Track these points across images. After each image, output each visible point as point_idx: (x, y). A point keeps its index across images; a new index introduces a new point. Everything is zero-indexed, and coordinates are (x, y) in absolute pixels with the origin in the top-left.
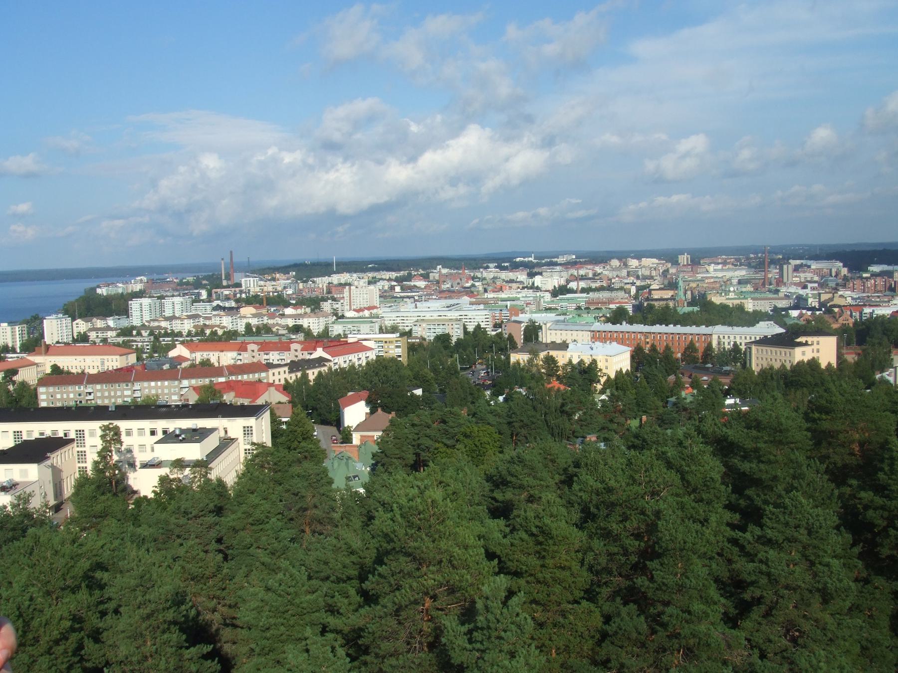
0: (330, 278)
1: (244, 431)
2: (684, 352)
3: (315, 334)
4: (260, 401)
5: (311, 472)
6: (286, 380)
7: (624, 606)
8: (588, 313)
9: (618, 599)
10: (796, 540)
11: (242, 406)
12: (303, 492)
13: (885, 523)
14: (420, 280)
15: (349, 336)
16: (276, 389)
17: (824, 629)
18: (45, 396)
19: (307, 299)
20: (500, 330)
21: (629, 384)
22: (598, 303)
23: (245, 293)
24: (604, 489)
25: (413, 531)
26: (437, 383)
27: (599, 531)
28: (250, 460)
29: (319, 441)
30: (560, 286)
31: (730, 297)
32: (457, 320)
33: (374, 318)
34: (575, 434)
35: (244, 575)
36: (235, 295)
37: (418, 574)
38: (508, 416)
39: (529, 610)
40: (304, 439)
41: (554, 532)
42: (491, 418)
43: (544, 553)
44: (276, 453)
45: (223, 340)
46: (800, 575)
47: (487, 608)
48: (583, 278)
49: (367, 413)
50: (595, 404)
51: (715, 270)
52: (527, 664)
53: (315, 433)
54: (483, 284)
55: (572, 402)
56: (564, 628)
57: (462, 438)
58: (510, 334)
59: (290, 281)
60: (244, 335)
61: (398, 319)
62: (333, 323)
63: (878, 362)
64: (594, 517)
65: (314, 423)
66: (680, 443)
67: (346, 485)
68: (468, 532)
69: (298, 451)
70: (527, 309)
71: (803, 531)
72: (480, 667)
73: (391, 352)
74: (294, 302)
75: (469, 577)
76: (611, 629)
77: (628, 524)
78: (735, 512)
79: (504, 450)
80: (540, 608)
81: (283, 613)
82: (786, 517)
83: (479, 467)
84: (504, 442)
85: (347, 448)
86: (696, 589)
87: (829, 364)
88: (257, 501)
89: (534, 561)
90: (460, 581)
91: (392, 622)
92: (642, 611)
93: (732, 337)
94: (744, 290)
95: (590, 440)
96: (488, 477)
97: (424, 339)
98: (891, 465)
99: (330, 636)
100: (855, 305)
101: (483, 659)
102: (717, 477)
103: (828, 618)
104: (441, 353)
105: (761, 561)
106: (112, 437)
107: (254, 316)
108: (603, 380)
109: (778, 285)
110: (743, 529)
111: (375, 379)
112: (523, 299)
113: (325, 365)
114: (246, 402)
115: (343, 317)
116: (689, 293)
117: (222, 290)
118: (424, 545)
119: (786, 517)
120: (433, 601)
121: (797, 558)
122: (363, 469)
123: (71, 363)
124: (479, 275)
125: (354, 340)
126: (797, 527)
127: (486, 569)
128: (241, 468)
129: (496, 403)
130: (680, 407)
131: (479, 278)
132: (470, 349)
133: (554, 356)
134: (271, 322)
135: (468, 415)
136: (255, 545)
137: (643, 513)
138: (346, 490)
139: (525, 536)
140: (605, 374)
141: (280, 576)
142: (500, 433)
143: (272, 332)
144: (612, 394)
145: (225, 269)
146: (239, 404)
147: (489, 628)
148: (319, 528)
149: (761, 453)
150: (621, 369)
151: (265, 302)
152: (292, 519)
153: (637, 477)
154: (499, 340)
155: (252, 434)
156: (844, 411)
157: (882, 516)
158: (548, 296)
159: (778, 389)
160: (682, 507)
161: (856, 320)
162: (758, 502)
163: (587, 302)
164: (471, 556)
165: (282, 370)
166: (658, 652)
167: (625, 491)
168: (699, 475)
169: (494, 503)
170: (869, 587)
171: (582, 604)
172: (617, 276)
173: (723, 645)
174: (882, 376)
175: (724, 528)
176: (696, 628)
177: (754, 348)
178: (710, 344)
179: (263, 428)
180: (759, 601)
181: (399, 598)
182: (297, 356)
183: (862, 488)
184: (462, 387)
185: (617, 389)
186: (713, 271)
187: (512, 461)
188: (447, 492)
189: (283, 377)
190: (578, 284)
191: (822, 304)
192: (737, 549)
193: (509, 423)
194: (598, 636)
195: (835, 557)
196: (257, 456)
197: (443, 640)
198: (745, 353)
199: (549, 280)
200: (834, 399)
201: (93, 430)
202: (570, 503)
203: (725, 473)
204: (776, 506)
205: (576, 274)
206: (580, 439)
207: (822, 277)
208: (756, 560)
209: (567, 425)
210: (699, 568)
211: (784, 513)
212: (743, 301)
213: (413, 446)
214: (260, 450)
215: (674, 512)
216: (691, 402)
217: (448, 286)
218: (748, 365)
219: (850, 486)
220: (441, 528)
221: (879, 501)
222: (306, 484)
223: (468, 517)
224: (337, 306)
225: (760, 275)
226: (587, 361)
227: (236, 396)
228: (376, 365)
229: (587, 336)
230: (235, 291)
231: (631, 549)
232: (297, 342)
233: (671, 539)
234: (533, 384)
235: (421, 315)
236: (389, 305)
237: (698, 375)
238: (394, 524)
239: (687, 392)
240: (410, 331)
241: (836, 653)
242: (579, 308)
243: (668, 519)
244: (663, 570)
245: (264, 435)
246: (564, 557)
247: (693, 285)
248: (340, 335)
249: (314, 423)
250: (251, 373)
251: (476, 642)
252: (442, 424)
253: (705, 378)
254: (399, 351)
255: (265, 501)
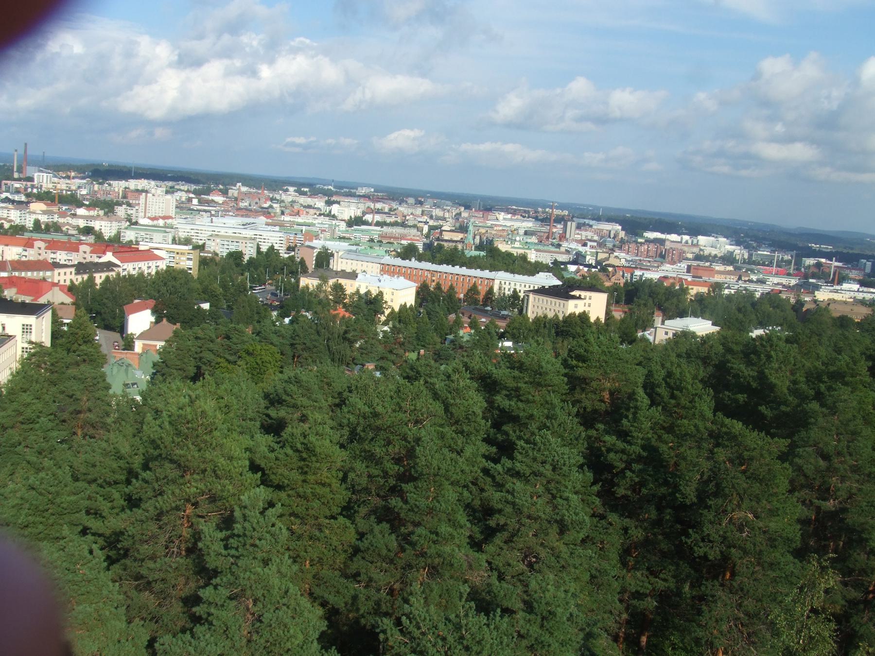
0: (127, 183)
1: (23, 329)
2: (467, 293)
3: (106, 238)
4: (42, 300)
5: (88, 375)
6: (71, 281)
7: (378, 525)
8: (380, 246)
9: (373, 518)
10: (541, 475)
11: (23, 304)
12: (78, 394)
13: (623, 466)
14: (219, 195)
15: (141, 243)
16: (61, 290)
17: (558, 557)
19: (101, 202)
20: (293, 253)
21: (411, 318)
22: (391, 238)
23: (37, 188)
24: (371, 413)
25: (180, 439)
26: (225, 299)
27: (363, 454)
28: (26, 359)
29: (101, 346)
30: (355, 217)
31: (516, 246)
32: (251, 239)
33: (168, 228)
34: (355, 361)
35: (9, 473)
36: (26, 189)
37: (181, 481)
38: (292, 337)
39: (288, 522)
40: (85, 342)
41: (318, 450)
42: (275, 339)
43: (306, 469)
44: (53, 354)
45: (9, 233)
46: (541, 507)
47: (245, 517)
48: (379, 212)
49: (151, 322)
50: (377, 334)
51: (504, 219)
52: (279, 572)
53: (97, 338)
54: (281, 207)
55: (355, 330)
56: (319, 541)
57: (244, 355)
58: (302, 259)
59: (85, 181)
60: (31, 231)
61: (193, 231)
62: (126, 228)
63: (641, 321)
64: (361, 440)
65: (96, 327)
66: (449, 377)
67: (123, 391)
68: (236, 445)
69: (77, 353)
70: (322, 236)
71: (548, 466)
72: (234, 572)
73: (181, 263)
74: (87, 203)
75: (230, 487)
76: (364, 545)
77: (390, 448)
78: (492, 446)
79: (284, 370)
80: (298, 521)
81: (43, 512)
82: (535, 453)
83: (258, 385)
84: (285, 363)
85: (128, 355)
86: (445, 513)
87: (598, 319)
88: (29, 400)
89: (296, 476)
90: (222, 491)
91: (153, 527)
92: (394, 529)
93: (512, 284)
94: (529, 241)
95: (368, 368)
96: (265, 395)
97: (217, 254)
98: (635, 414)
99: (90, 537)
100: (628, 267)
101: (237, 565)
102: (479, 412)
103: (564, 549)
104: (233, 270)
105: (508, 491)
107: (44, 212)
108: (387, 312)
109: (560, 240)
110: (496, 461)
111: (164, 289)
112: (319, 225)
113: (113, 270)
114: (28, 300)
115: (136, 223)
116: (478, 237)
117: (13, 182)
118: (189, 453)
119: (535, 453)
120: (195, 508)
121: (540, 490)
122: (142, 377)
124: (278, 197)
125: (146, 248)
126: (544, 462)
127: (249, 481)
128: (15, 366)
129: (281, 324)
130: (457, 345)
131: (278, 200)
132: (262, 269)
133: (343, 284)
134: (61, 220)
135: (253, 334)
136: (23, 444)
137: (405, 438)
138: (122, 396)
139: (289, 451)
140: (390, 307)
141: (42, 474)
142: (282, 354)
143: (62, 231)
144: (394, 327)
145: (18, 161)
146: (20, 300)
147: (245, 535)
148: (92, 431)
149: (521, 392)
150: (405, 303)
151: (57, 200)
152: (64, 421)
153: (403, 405)
154: (291, 263)
155: (31, 332)
156: (599, 361)
157: (621, 459)
158: (343, 226)
159: (549, 336)
160: (442, 436)
161: (627, 281)
162: (513, 437)
163: (380, 236)
164: (235, 468)
165: (68, 270)
166: (404, 568)
167: (390, 417)
168: (462, 408)
169: (268, 420)
170: (603, 522)
171: (339, 520)
172: (412, 214)
173: (465, 566)
174: (643, 335)
175: (480, 459)
176: (442, 548)
177: (531, 296)
178: (491, 289)
179: (44, 327)
180: (501, 528)
181: (161, 503)
182: (85, 258)
183: (607, 432)
184: (250, 305)
185: (400, 321)
186: (503, 219)
187: (289, 381)
188: (219, 405)
189: (68, 278)
190: (373, 218)
191: (598, 263)
192: (490, 479)
193: (292, 345)
194: (350, 550)
195: (576, 493)
196: (34, 355)
197: (200, 545)
198: (523, 300)
199: (346, 209)
200: (591, 349)
202: (340, 425)
203: (486, 408)
204: (527, 442)
205: (372, 207)
206: (359, 366)
207: (602, 237)
208: (504, 490)
209: (348, 352)
210: (451, 494)
211: (534, 449)
212: (526, 251)
213: (195, 358)
214: (38, 349)
215: (432, 440)
216: (468, 341)
217: (247, 204)
218: (524, 311)
219: (597, 430)
220: (208, 438)
221: (620, 445)
222: (82, 387)
223: (238, 430)
224: (132, 212)
225: (545, 229)
226: (374, 293)
227: (18, 293)
228: (165, 275)
229: (377, 268)
230: (26, 185)
231: (391, 473)
232: (86, 244)
233: (426, 465)
234: (319, 308)
235: (216, 230)
236: (185, 216)
237: (477, 316)
238: (161, 431)
239: (465, 331)
240: (204, 245)
241: (567, 579)
242: (372, 240)
243: (426, 445)
244: (417, 492)
245: (43, 335)
246: (325, 474)
247: (483, 231)
248: (131, 241)
249: (96, 327)
250: (36, 270)
251: (232, 548)
252: (226, 340)
253: (483, 320)
254: (190, 264)
255: (38, 401)
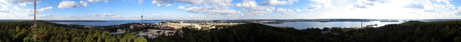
18: (160, 28)
106: (165, 31)
123: (161, 26)
201: (163, 31)
